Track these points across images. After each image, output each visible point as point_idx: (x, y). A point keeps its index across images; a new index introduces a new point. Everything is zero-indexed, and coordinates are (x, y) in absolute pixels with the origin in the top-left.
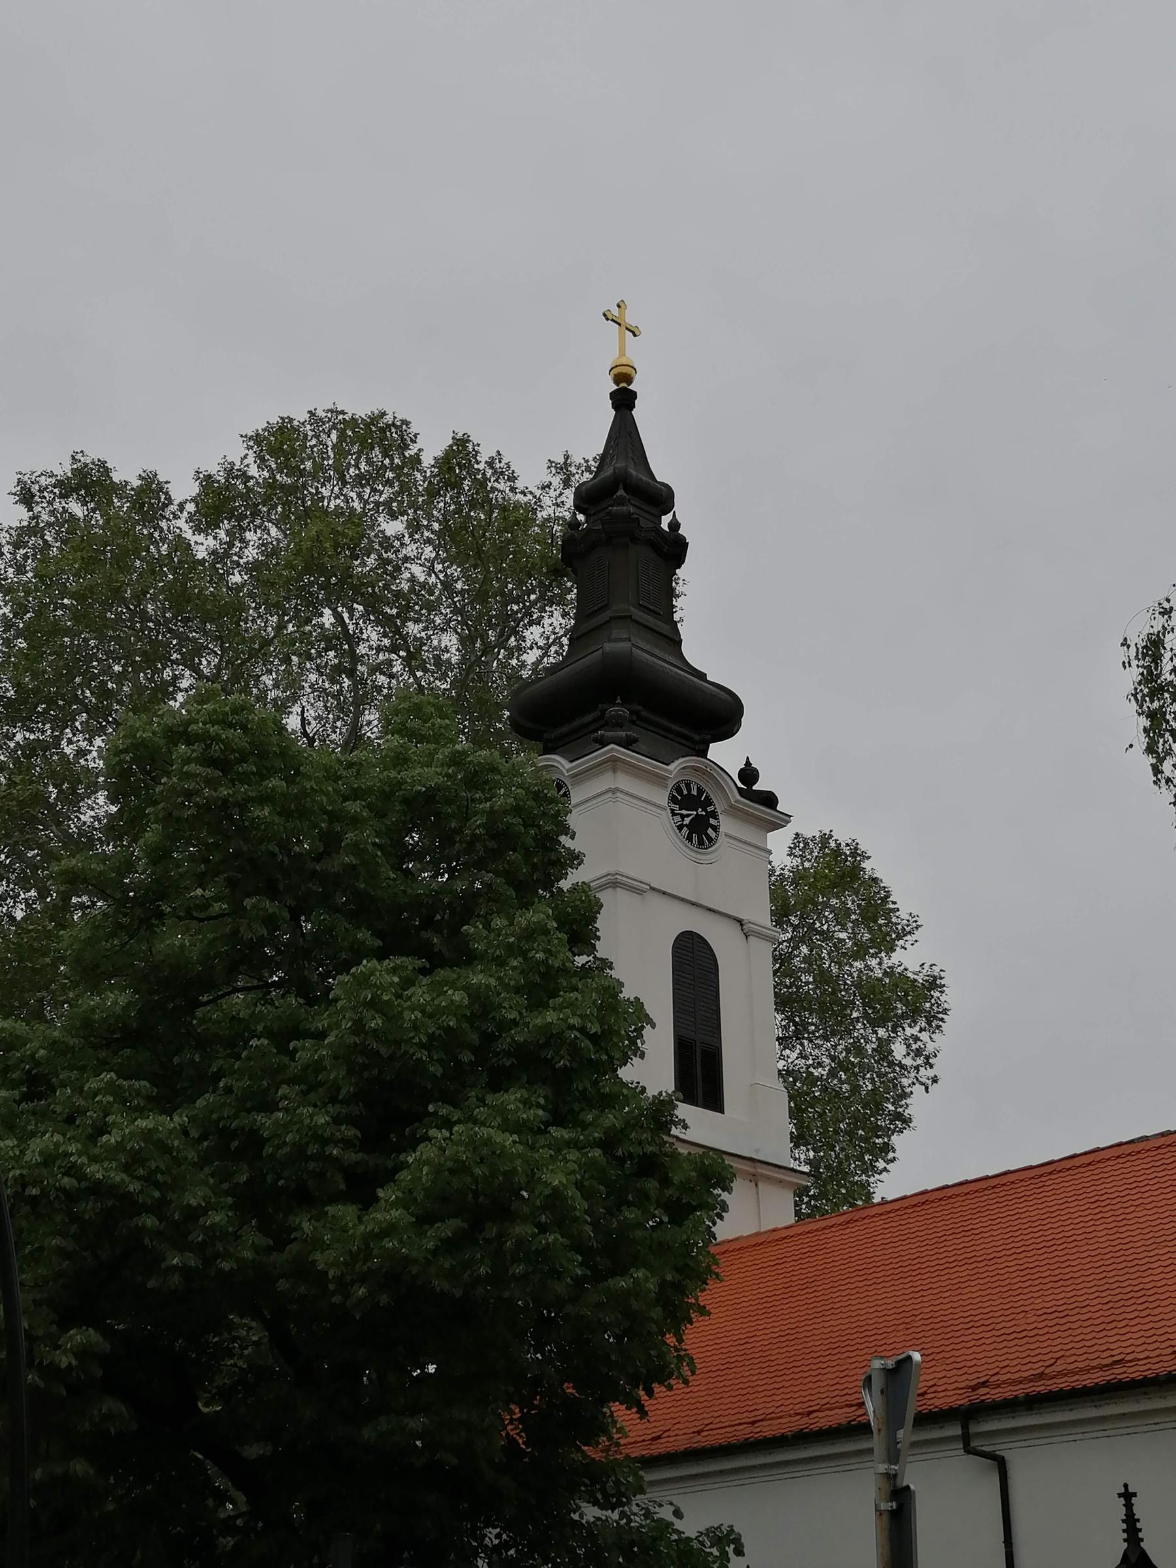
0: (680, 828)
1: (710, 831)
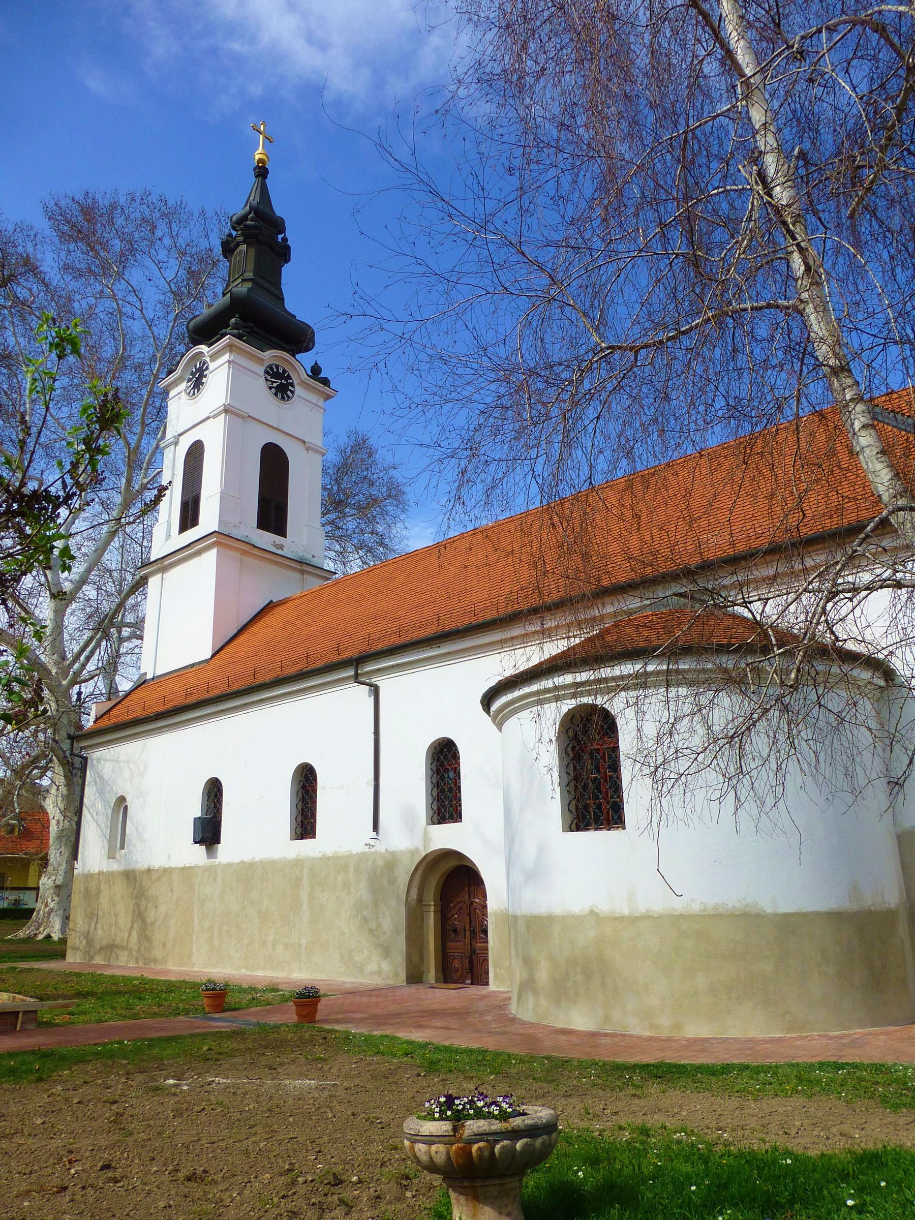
0: (270, 388)
1: (289, 393)
